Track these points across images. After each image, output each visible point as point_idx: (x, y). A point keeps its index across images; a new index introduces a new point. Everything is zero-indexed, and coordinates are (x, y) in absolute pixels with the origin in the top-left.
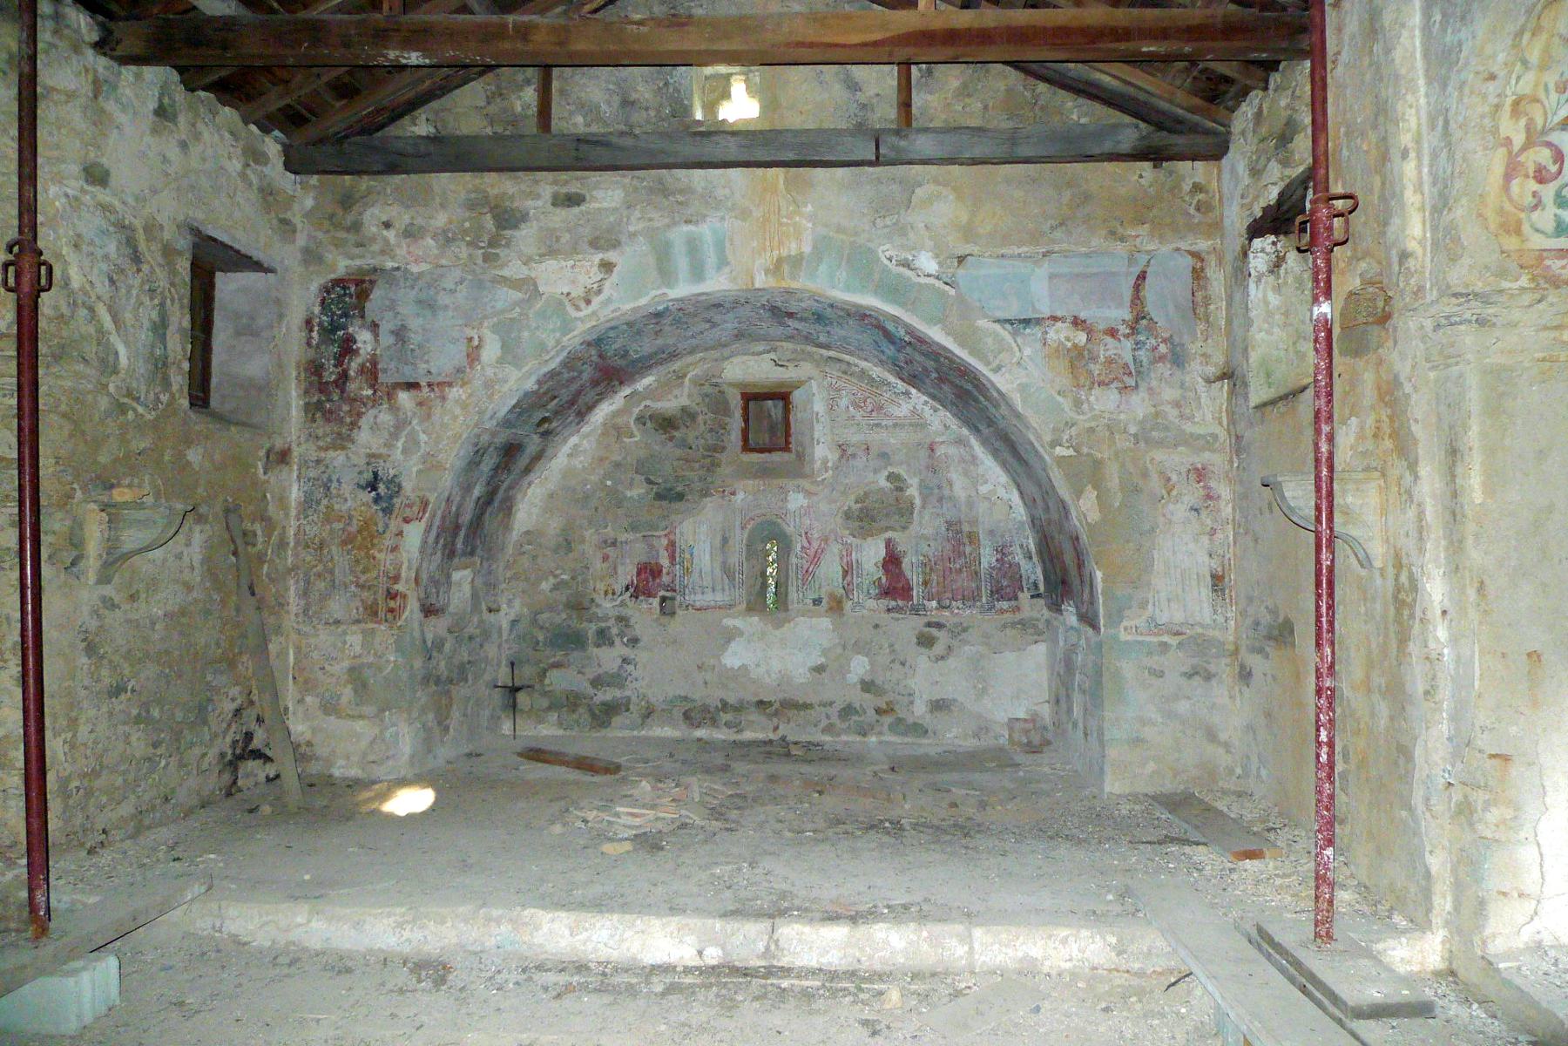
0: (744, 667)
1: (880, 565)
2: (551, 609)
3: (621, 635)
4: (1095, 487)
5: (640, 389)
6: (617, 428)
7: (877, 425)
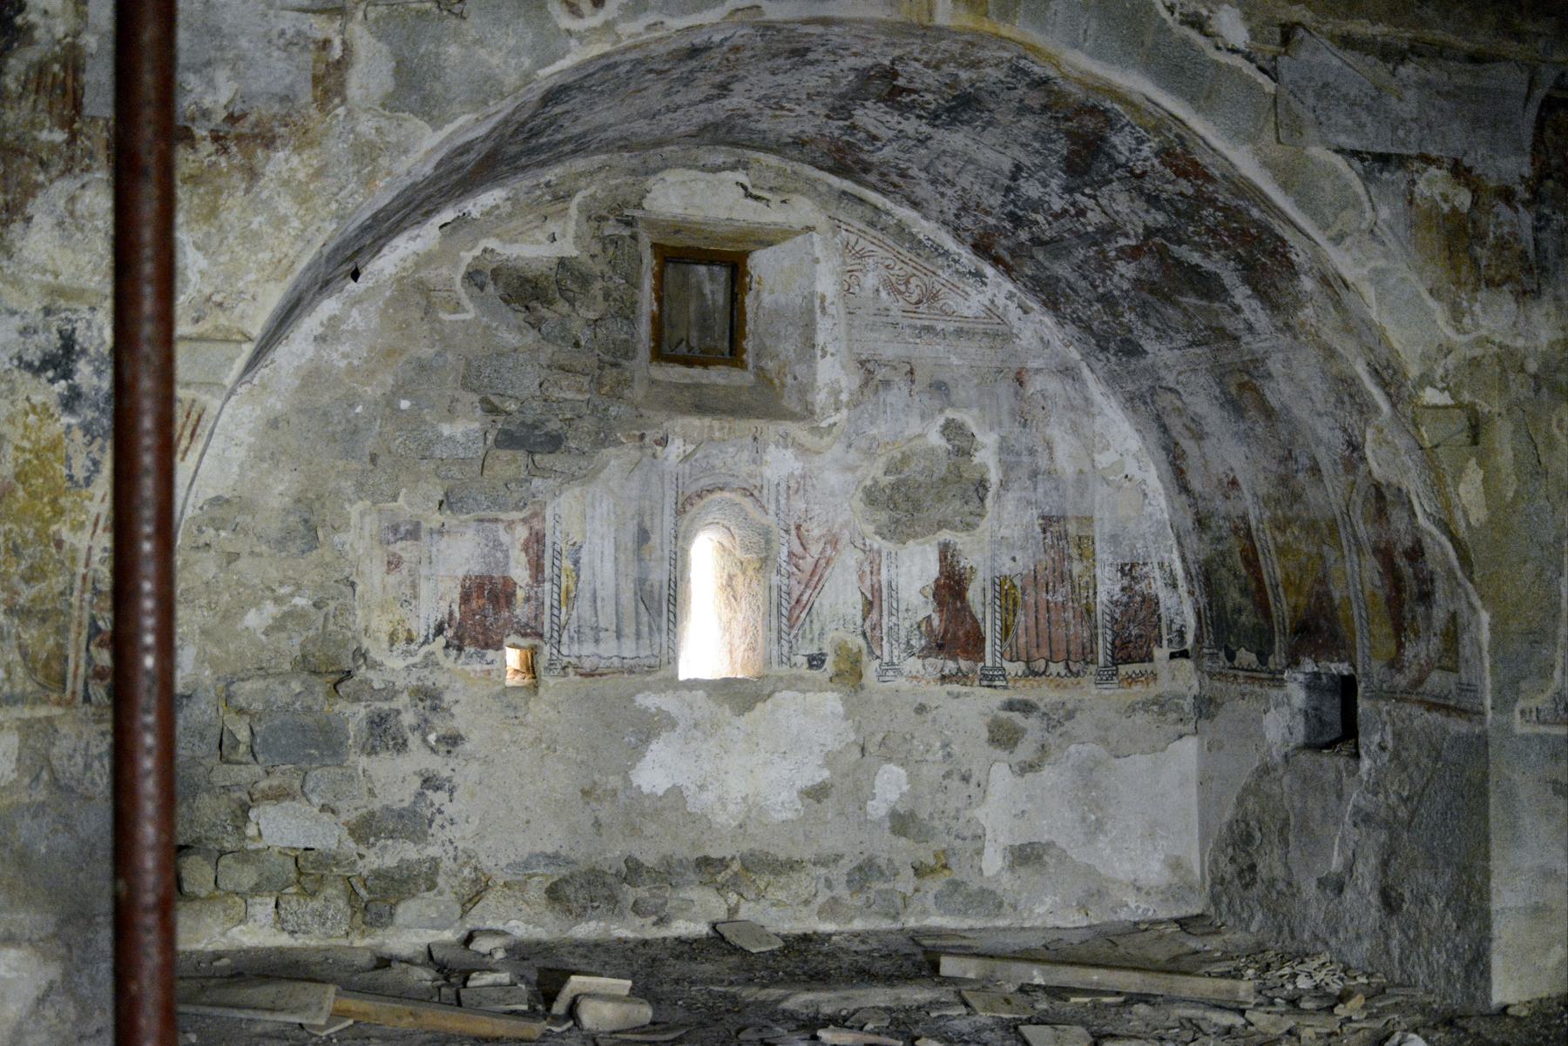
0: (676, 792)
1: (929, 592)
2: (263, 672)
3: (423, 727)
4: (1480, 464)
5: (475, 214)
6: (423, 288)
7: (929, 329)
